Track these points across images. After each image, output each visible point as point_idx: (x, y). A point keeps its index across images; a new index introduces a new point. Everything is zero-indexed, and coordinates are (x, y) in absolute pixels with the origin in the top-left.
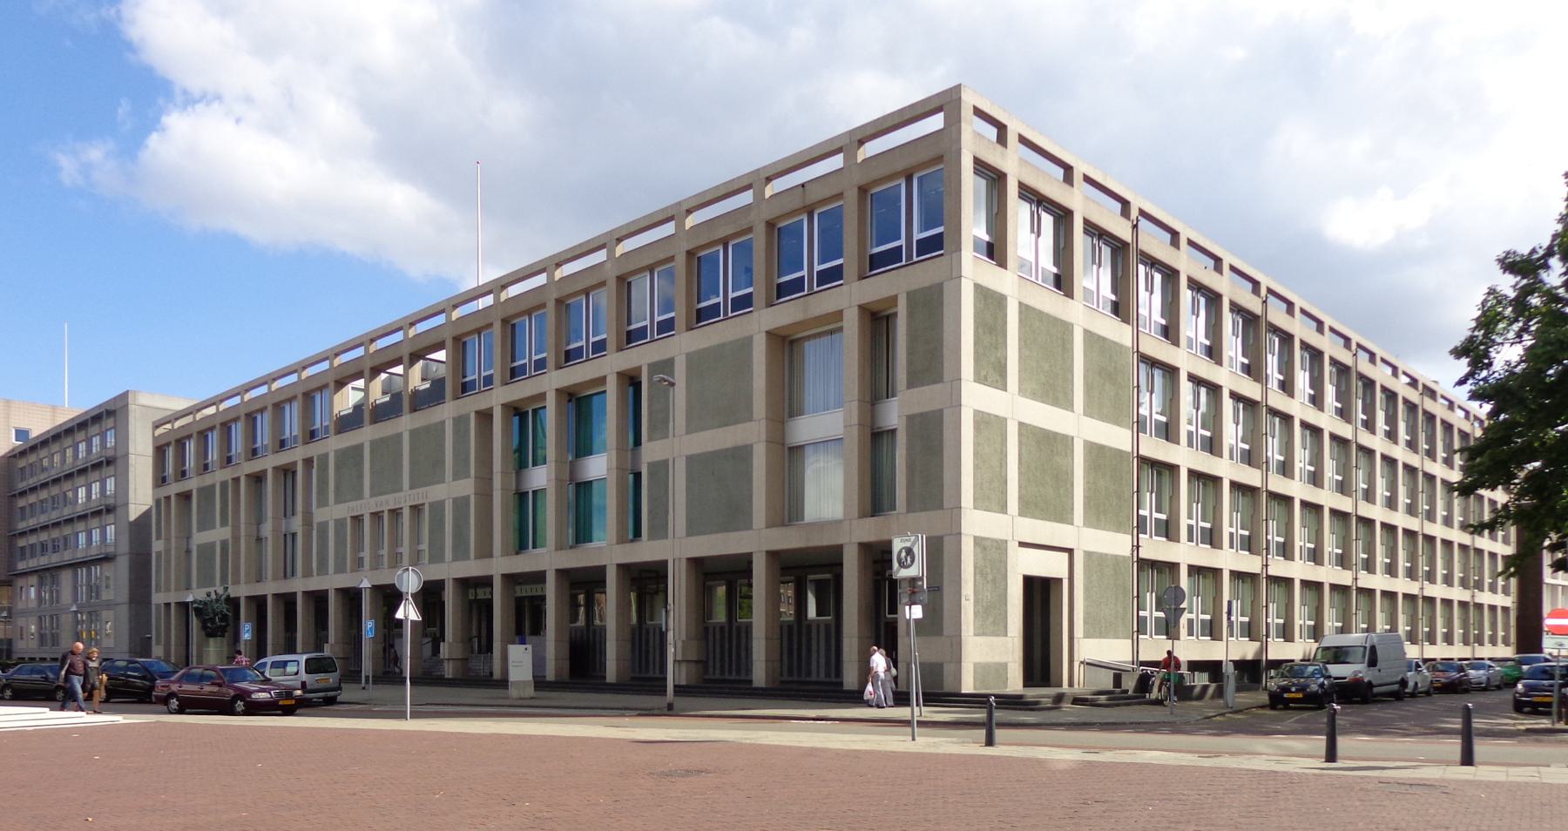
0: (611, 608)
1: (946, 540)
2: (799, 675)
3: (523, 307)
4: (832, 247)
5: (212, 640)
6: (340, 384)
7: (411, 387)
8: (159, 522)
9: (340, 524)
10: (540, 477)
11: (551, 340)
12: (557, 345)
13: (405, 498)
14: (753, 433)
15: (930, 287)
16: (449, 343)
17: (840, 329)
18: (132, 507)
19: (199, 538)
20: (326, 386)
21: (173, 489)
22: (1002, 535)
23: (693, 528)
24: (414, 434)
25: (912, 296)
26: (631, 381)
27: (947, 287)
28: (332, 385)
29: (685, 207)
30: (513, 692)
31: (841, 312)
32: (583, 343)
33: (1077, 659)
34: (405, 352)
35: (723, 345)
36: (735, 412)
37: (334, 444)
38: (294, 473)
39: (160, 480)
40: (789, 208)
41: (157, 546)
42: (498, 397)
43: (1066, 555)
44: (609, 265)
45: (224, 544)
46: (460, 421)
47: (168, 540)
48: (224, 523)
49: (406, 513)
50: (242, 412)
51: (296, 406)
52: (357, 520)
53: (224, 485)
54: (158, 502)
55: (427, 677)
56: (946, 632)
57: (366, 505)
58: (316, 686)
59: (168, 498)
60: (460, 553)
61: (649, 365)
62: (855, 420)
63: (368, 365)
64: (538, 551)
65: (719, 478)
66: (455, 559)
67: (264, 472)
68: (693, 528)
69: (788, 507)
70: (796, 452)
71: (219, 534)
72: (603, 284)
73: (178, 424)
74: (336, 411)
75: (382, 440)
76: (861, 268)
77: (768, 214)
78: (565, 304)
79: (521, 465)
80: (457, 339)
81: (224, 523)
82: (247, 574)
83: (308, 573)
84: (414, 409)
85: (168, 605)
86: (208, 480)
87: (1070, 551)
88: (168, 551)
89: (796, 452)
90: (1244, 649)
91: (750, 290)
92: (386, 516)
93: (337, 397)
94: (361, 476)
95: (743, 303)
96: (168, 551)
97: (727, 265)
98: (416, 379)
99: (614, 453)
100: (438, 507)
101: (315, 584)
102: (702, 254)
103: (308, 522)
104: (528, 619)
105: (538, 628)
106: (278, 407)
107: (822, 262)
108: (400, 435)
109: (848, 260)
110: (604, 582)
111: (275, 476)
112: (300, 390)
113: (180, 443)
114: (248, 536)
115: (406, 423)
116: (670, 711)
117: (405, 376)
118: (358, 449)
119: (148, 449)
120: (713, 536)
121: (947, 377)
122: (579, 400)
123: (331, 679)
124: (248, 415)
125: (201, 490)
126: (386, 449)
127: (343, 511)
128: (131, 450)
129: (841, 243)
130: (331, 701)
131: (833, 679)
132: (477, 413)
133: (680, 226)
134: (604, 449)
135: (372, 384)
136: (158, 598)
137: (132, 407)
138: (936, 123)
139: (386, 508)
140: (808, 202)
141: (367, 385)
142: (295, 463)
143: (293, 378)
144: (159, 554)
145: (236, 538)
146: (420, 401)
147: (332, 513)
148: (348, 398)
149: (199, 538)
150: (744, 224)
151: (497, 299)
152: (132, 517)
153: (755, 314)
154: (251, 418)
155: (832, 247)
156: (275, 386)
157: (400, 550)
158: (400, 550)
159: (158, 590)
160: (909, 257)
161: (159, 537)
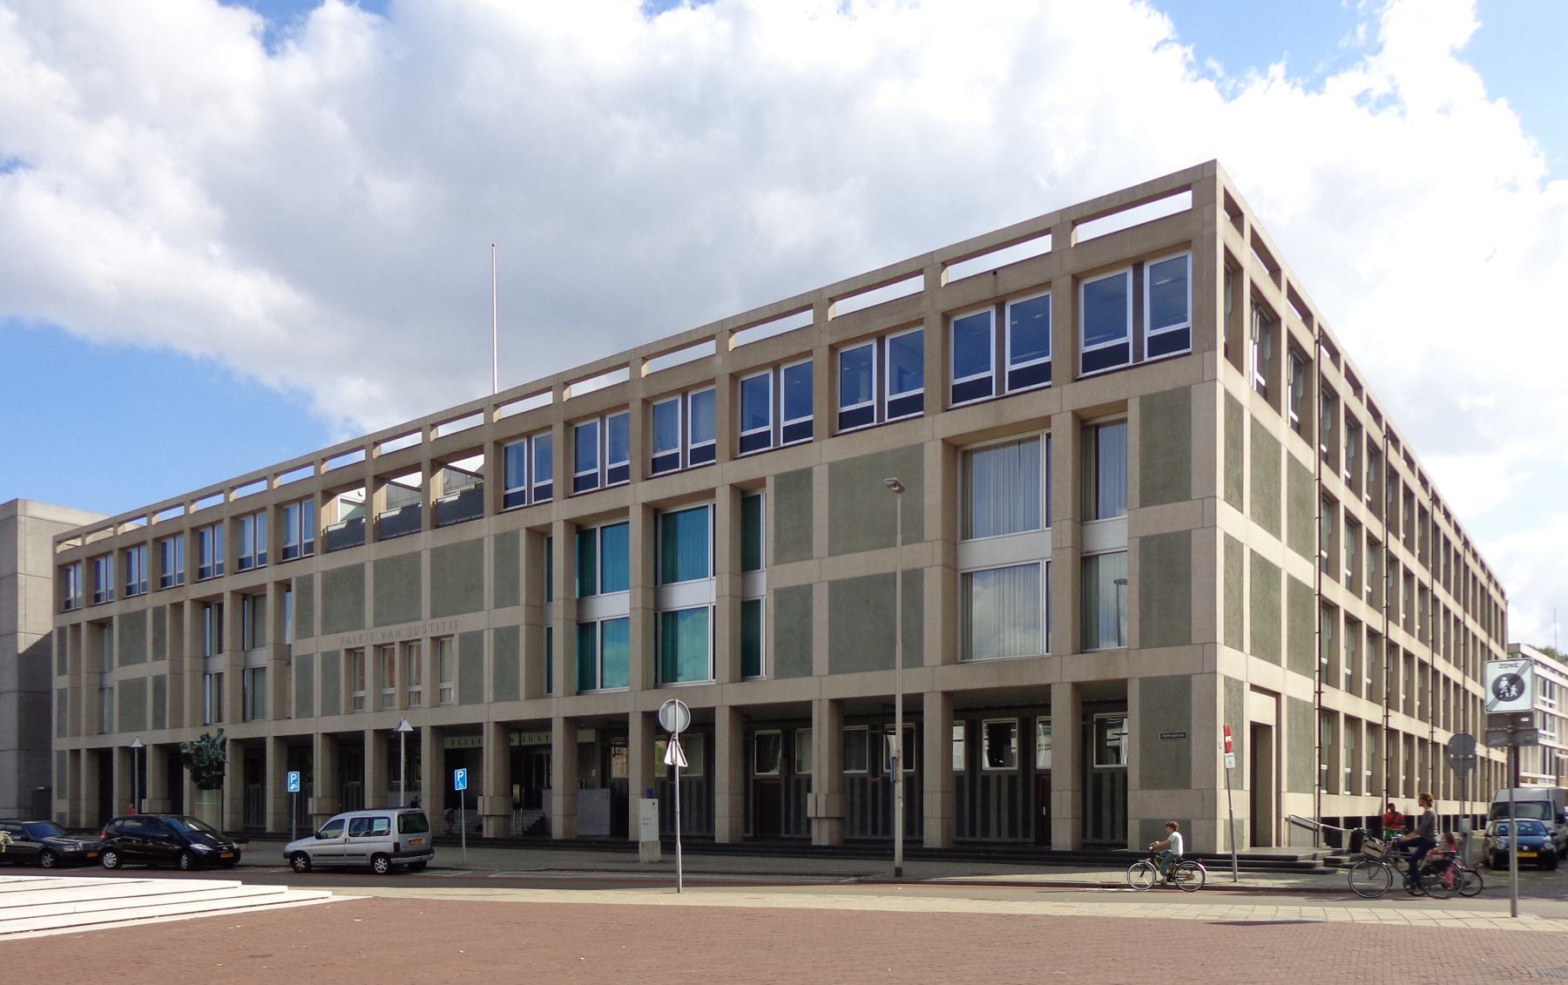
0: (819, 754)
1: (1196, 683)
2: (973, 834)
3: (597, 408)
4: (799, 401)
5: (205, 793)
6: (328, 495)
7: (432, 499)
8: (62, 654)
9: (330, 659)
10: (612, 605)
11: (636, 444)
12: (644, 451)
13: (424, 628)
14: (927, 555)
15: (1173, 391)
16: (489, 447)
17: (1125, 421)
18: (21, 636)
19: (119, 674)
20: (311, 496)
21: (85, 616)
22: (1255, 680)
23: (837, 665)
24: (436, 553)
25: (1147, 402)
26: (747, 500)
27: (1196, 391)
28: (319, 496)
29: (939, 259)
30: (644, 855)
31: (1126, 401)
32: (525, 488)
33: (1286, 813)
34: (425, 457)
35: (881, 454)
36: (915, 533)
37: (320, 565)
38: (221, 606)
39: (63, 605)
40: (973, 299)
41: (59, 682)
42: (559, 513)
43: (1273, 700)
44: (719, 360)
45: (159, 683)
46: (505, 542)
47: (76, 674)
48: (159, 654)
49: (426, 646)
50: (149, 537)
51: (81, 569)
52: (354, 654)
53: (159, 612)
54: (61, 631)
55: (701, 843)
56: (1194, 785)
57: (368, 636)
58: (410, 849)
59: (76, 627)
60: (505, 689)
61: (777, 477)
62: (727, 591)
63: (371, 471)
64: (604, 691)
65: (871, 613)
66: (497, 699)
67: (110, 619)
68: (837, 665)
69: (960, 646)
70: (968, 577)
71: (150, 669)
72: (263, 509)
73: (90, 539)
74: (323, 527)
75: (393, 561)
76: (732, 448)
77: (944, 304)
78: (576, 426)
79: (587, 590)
80: (498, 444)
81: (159, 654)
82: (567, 681)
83: (282, 715)
84: (436, 525)
85: (76, 753)
86: (134, 605)
87: (1277, 695)
88: (76, 689)
89: (968, 577)
90: (1366, 806)
91: (809, 418)
92: (397, 648)
93: (325, 510)
94: (360, 602)
95: (620, 475)
96: (76, 689)
97: (602, 434)
98: (441, 489)
99: (639, 590)
100: (471, 642)
101: (293, 728)
102: (657, 403)
103: (283, 654)
104: (209, 778)
105: (217, 783)
106: (125, 552)
107: (1153, 327)
108: (417, 555)
109: (818, 416)
110: (1125, 701)
111: (234, 603)
112: (270, 502)
113: (93, 562)
114: (192, 671)
115: (425, 541)
116: (899, 878)
117: (423, 489)
118: (357, 571)
119: (47, 570)
120: (869, 674)
121: (1196, 492)
122: (665, 516)
123: (423, 839)
124: (194, 530)
125: (123, 617)
126: (398, 574)
127: (337, 642)
128: (20, 569)
129: (811, 399)
130: (419, 867)
131: (879, 836)
132: (528, 529)
133: (270, 485)
134: (622, 585)
135: (376, 495)
136: (60, 744)
137: (21, 519)
138: (1182, 202)
139: (397, 640)
140: (1001, 291)
141: (426, 481)
142: (221, 595)
143: (261, 486)
144: (62, 693)
145: (177, 675)
146: (443, 516)
147: (319, 645)
148: (337, 513)
149: (119, 674)
150: (912, 315)
151: (558, 397)
152: (22, 648)
153: (928, 420)
154: (160, 544)
155: (799, 401)
156: (234, 496)
157: (445, 685)
158: (445, 685)
159: (61, 733)
160: (881, 417)
161: (62, 672)
